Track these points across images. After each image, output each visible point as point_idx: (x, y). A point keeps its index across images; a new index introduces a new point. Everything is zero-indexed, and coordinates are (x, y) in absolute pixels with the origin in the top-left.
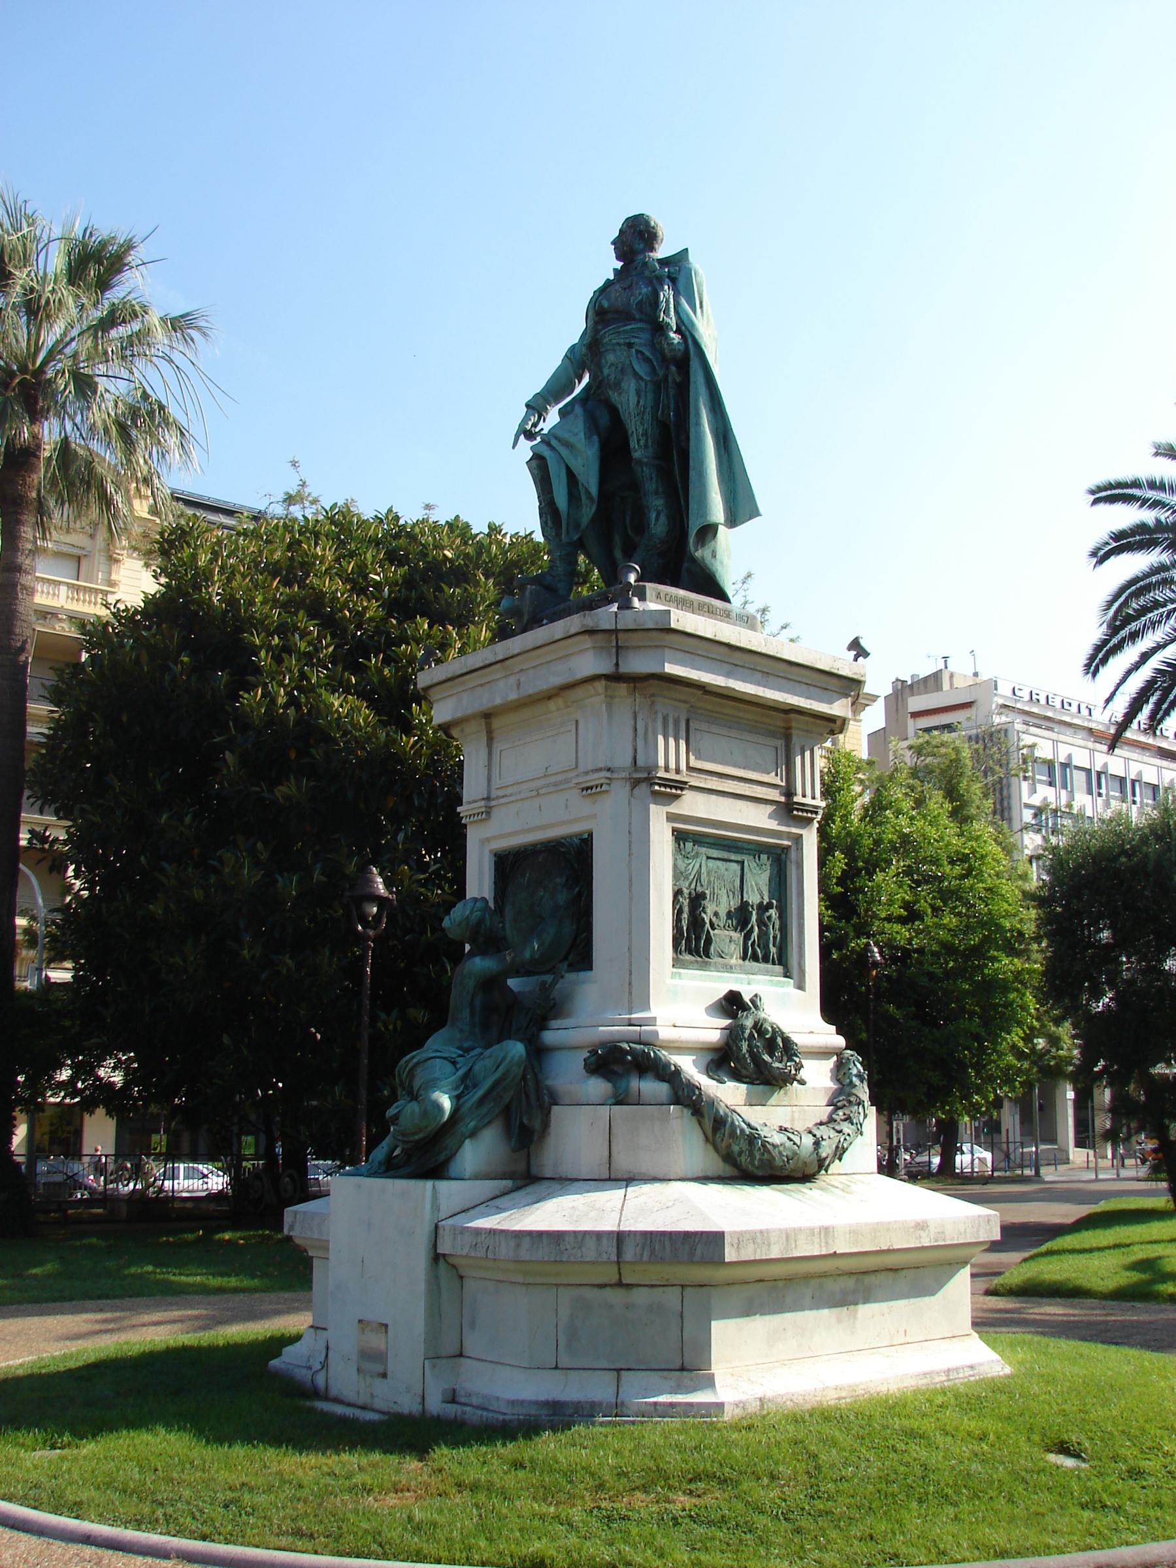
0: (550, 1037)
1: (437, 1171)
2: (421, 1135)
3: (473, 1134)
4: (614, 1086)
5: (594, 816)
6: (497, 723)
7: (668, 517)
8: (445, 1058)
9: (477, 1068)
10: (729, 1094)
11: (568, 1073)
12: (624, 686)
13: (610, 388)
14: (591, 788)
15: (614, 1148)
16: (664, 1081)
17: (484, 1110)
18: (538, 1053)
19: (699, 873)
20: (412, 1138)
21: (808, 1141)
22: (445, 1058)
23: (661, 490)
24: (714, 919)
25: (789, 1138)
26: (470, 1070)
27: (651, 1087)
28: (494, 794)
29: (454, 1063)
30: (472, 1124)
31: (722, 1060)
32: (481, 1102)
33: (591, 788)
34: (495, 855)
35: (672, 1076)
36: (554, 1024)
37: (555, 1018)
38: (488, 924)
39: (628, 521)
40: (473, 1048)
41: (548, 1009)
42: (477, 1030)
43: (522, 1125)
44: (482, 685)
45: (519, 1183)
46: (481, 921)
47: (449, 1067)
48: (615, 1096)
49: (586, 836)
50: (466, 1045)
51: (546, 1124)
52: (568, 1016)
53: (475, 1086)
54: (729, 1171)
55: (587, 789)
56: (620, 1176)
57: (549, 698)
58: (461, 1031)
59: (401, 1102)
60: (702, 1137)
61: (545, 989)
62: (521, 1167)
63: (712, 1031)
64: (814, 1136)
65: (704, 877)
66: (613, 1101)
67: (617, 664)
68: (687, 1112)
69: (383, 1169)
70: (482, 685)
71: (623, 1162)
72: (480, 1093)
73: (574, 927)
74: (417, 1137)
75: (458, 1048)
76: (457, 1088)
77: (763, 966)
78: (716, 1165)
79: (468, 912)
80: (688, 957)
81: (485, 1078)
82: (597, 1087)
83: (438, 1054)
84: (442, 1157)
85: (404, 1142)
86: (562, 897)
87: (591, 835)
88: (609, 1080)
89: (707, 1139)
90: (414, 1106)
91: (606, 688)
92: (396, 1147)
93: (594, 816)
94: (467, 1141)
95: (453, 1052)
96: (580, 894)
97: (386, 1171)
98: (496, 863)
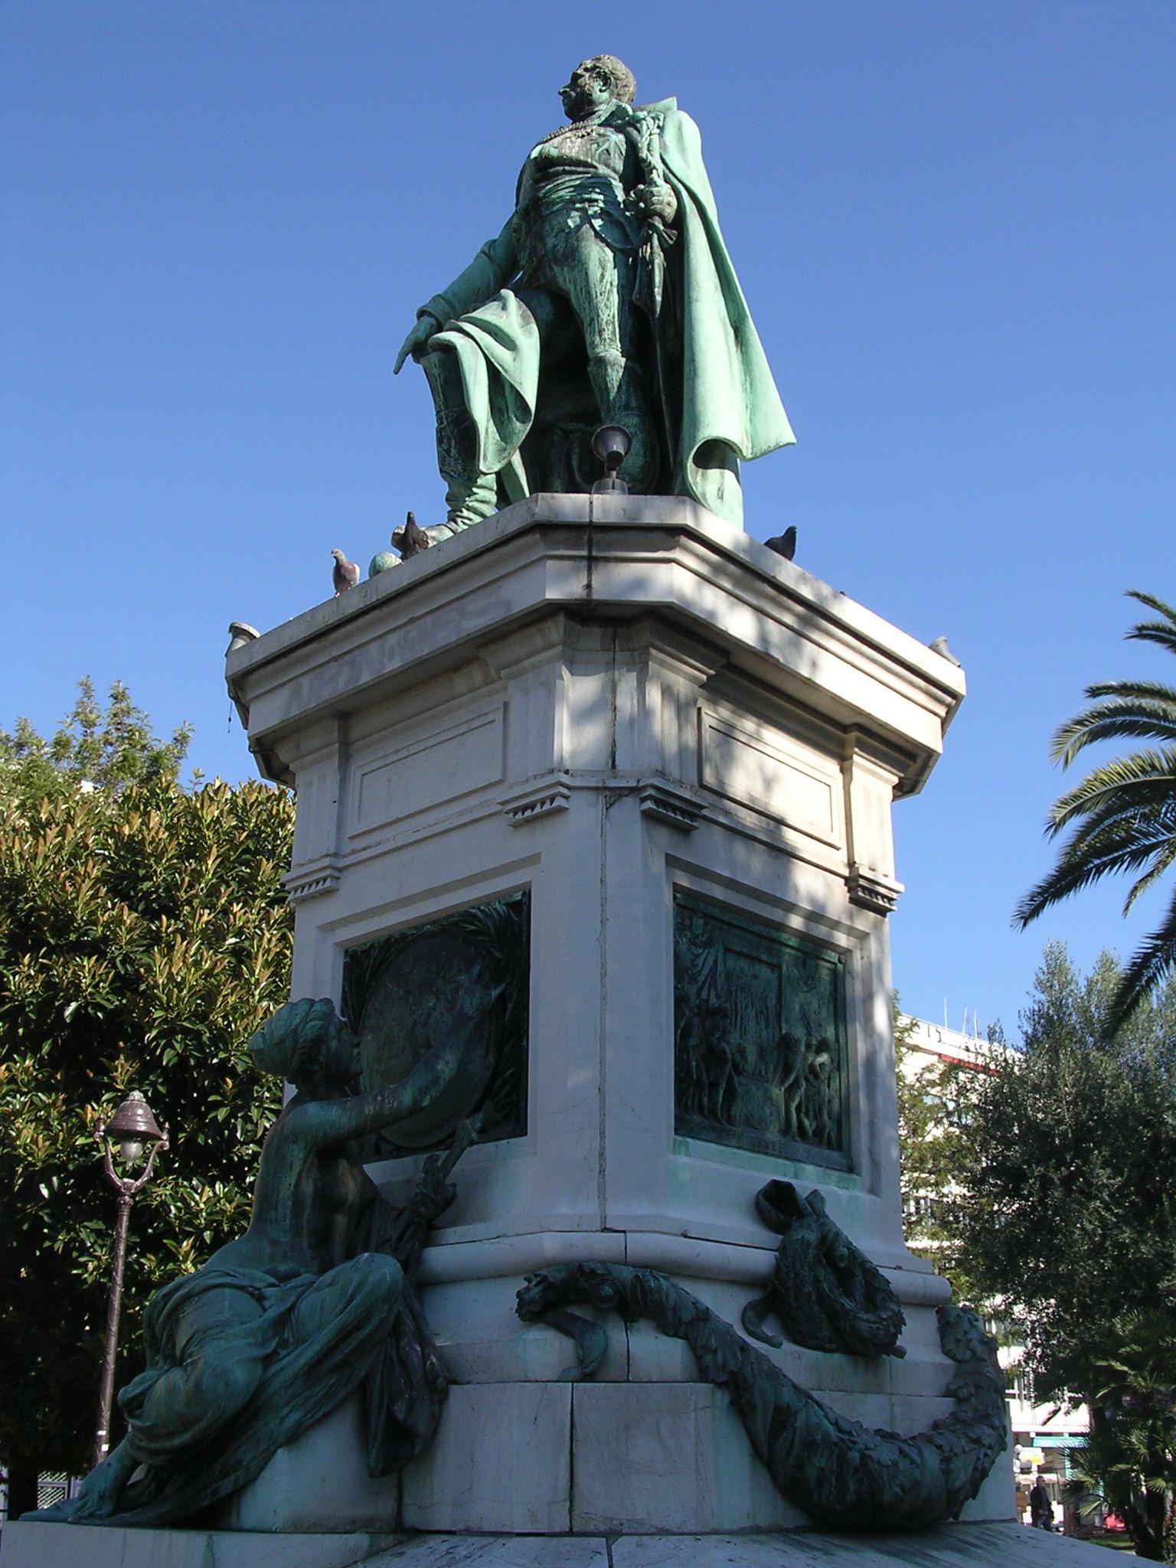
0: (442, 1256)
1: (212, 1514)
2: (187, 1436)
3: (293, 1438)
4: (580, 1344)
5: (534, 859)
6: (358, 729)
7: (644, 444)
8: (242, 1288)
9: (304, 1306)
10: (794, 1361)
11: (477, 1320)
12: (596, 631)
13: (556, 260)
14: (532, 807)
15: (579, 1467)
16: (274, 1453)
17: (319, 1390)
18: (422, 1284)
19: (713, 971)
20: (167, 1445)
21: (932, 1459)
22: (242, 1288)
23: (634, 404)
24: (738, 1058)
25: (901, 1452)
26: (292, 1308)
27: (652, 1349)
28: (347, 848)
29: (260, 1298)
30: (294, 1417)
31: (774, 1298)
32: (312, 1371)
33: (532, 807)
34: (346, 952)
35: (688, 1325)
36: (452, 1234)
37: (453, 1223)
38: (334, 1044)
39: (574, 463)
40: (296, 1275)
41: (436, 1209)
42: (305, 1241)
43: (391, 1420)
44: (335, 659)
45: (385, 1541)
46: (319, 1040)
47: (248, 1304)
48: (581, 1362)
49: (518, 896)
50: (283, 1268)
51: (436, 1421)
52: (481, 1217)
53: (300, 1341)
54: (790, 1517)
55: (524, 809)
56: (592, 1527)
57: (456, 669)
58: (274, 1242)
59: (149, 1373)
60: (746, 1444)
61: (436, 1175)
62: (385, 1508)
63: (753, 1250)
64: (939, 1447)
65: (721, 981)
66: (575, 1373)
67: (589, 586)
68: (722, 1398)
69: (107, 1508)
70: (335, 659)
71: (600, 1499)
72: (309, 1352)
73: (491, 1059)
74: (177, 1442)
75: (267, 1272)
76: (263, 1343)
77: (815, 1150)
78: (769, 1508)
79: (297, 1021)
80: (697, 1118)
81: (321, 1326)
82: (546, 1349)
83: (228, 1280)
84: (227, 1486)
85: (153, 1453)
86: (471, 1002)
87: (527, 895)
88: (566, 1332)
89: (756, 1451)
90: (177, 1376)
91: (567, 632)
92: (136, 1464)
93: (534, 859)
94: (280, 1451)
95: (260, 1278)
96: (502, 999)
97: (113, 1513)
98: (346, 966)
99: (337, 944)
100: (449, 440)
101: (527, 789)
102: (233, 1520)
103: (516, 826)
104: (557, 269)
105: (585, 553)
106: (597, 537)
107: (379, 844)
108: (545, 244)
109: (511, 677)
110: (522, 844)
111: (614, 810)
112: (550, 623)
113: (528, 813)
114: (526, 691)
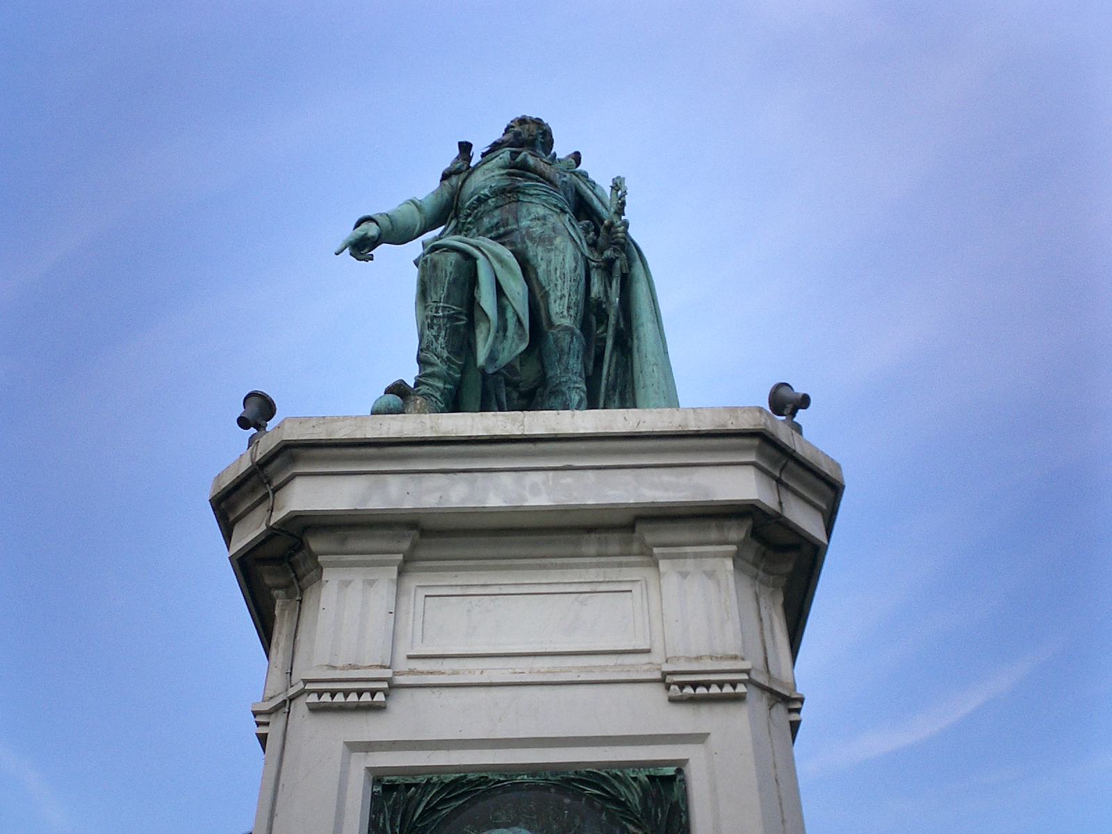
14: (707, 685)
49: (670, 771)
55: (695, 685)
99: (369, 769)
100: (439, 328)
101: (695, 667)
103: (672, 700)
104: (529, 244)
105: (777, 474)
106: (791, 464)
107: (455, 673)
108: (517, 221)
109: (665, 557)
110: (683, 720)
111: (774, 709)
112: (734, 523)
113: (701, 691)
114: (684, 575)
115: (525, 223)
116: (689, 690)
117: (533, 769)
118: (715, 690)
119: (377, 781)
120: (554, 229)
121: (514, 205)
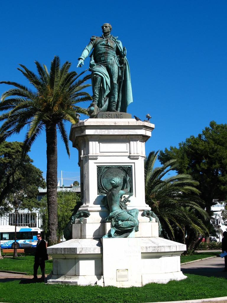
5: (134, 163)
14: (135, 157)
102: (128, 237)
104: (109, 65)
108: (107, 60)
115: (108, 60)
116: (133, 157)
117: (115, 166)
118: (136, 158)
119: (97, 166)
120: (113, 62)
121: (107, 56)
